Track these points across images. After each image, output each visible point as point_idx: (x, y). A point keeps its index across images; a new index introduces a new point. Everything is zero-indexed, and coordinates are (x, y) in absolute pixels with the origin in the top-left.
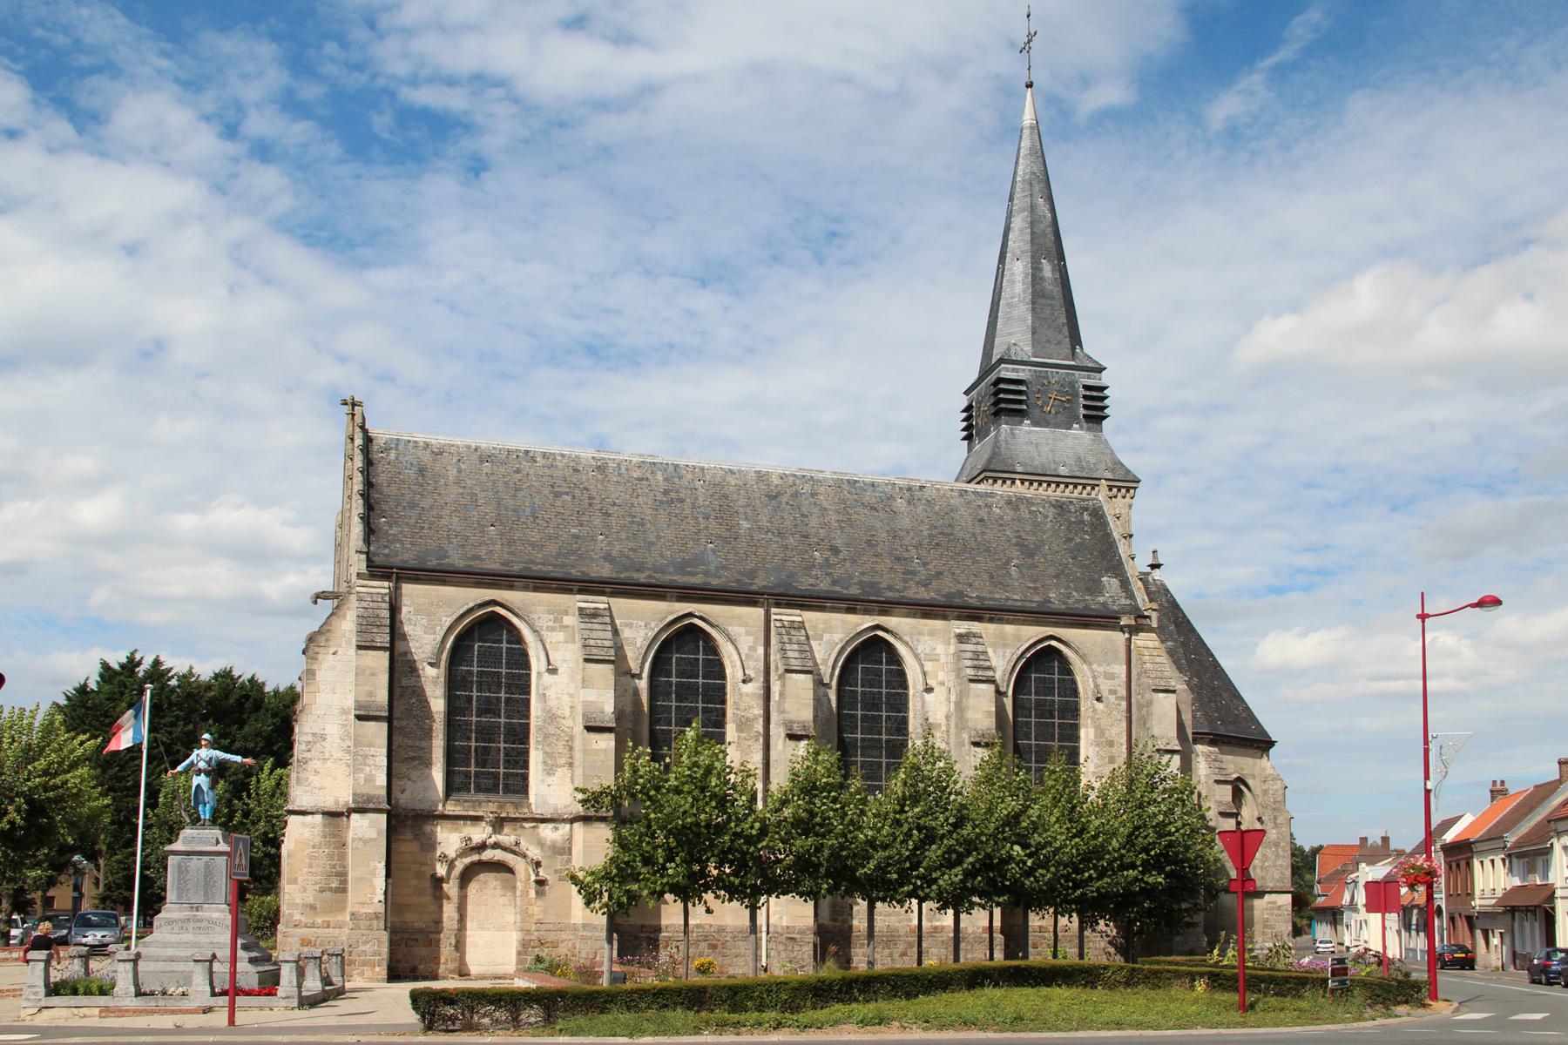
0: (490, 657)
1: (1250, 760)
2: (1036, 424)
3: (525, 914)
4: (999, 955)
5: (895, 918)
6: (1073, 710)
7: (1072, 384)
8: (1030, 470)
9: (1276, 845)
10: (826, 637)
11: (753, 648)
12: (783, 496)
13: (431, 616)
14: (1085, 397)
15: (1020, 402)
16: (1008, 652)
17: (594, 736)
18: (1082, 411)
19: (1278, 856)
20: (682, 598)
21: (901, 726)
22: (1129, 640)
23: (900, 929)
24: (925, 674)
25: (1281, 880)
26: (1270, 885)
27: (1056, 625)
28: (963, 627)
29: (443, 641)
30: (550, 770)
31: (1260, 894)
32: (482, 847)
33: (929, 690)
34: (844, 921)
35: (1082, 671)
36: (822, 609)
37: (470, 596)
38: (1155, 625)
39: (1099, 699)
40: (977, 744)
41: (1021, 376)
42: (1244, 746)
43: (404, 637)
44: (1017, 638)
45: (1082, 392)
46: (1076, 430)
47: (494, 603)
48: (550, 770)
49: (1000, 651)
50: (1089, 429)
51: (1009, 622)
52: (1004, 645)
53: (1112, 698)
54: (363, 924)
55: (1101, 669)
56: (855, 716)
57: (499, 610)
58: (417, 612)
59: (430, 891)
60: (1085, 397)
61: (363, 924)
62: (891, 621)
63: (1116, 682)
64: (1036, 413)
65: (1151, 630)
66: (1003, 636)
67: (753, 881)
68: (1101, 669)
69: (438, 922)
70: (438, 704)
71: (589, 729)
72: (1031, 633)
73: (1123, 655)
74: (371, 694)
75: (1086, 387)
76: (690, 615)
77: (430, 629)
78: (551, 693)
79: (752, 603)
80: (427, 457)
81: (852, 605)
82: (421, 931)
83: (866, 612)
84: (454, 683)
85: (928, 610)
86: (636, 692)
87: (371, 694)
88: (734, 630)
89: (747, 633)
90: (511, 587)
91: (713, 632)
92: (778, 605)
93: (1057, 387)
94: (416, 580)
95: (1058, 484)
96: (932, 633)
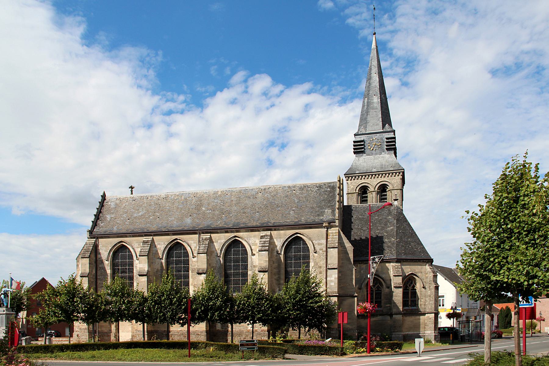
0: (124, 257)
1: (419, 267)
2: (368, 155)
3: (133, 328)
4: (146, 339)
5: (237, 327)
6: (308, 257)
7: (382, 139)
8: (361, 172)
9: (430, 296)
10: (219, 241)
11: (196, 247)
12: (199, 201)
13: (106, 247)
14: (387, 142)
15: (362, 148)
16: (282, 240)
17: (141, 277)
18: (386, 147)
19: (430, 300)
20: (174, 234)
21: (246, 267)
22: (327, 231)
23: (242, 330)
24: (252, 250)
25: (431, 309)
26: (428, 311)
27: (299, 229)
28: (263, 233)
29: (109, 253)
31: (424, 314)
33: (253, 255)
34: (226, 329)
35: (309, 243)
36: (217, 233)
37: (290, 232)
38: (337, 225)
39: (315, 253)
40: (199, 274)
41: (362, 139)
42: (415, 262)
43: (100, 254)
44: (285, 235)
45: (385, 140)
46: (383, 155)
47: (235, 236)
49: (279, 240)
50: (388, 154)
51: (282, 230)
52: (280, 238)
53: (321, 252)
54: (83, 331)
55: (317, 242)
56: (231, 265)
57: (298, 235)
58: (103, 246)
60: (387, 142)
61: (83, 331)
62: (240, 234)
63: (323, 246)
64: (367, 151)
65: (336, 226)
66: (280, 235)
67: (193, 318)
68: (317, 242)
69: (111, 330)
70: (109, 271)
71: (140, 275)
72: (290, 232)
73: (325, 236)
74: (85, 270)
75: (387, 139)
76: (176, 239)
77: (106, 251)
79: (195, 233)
80: (118, 202)
81: (227, 230)
82: (106, 333)
83: (232, 232)
84: (114, 265)
85: (253, 229)
86: (162, 263)
87: (85, 270)
88: (190, 242)
89: (194, 243)
90: (126, 237)
91: (128, 246)
92: (203, 233)
93: (376, 140)
94: (102, 238)
95: (372, 175)
96: (254, 236)
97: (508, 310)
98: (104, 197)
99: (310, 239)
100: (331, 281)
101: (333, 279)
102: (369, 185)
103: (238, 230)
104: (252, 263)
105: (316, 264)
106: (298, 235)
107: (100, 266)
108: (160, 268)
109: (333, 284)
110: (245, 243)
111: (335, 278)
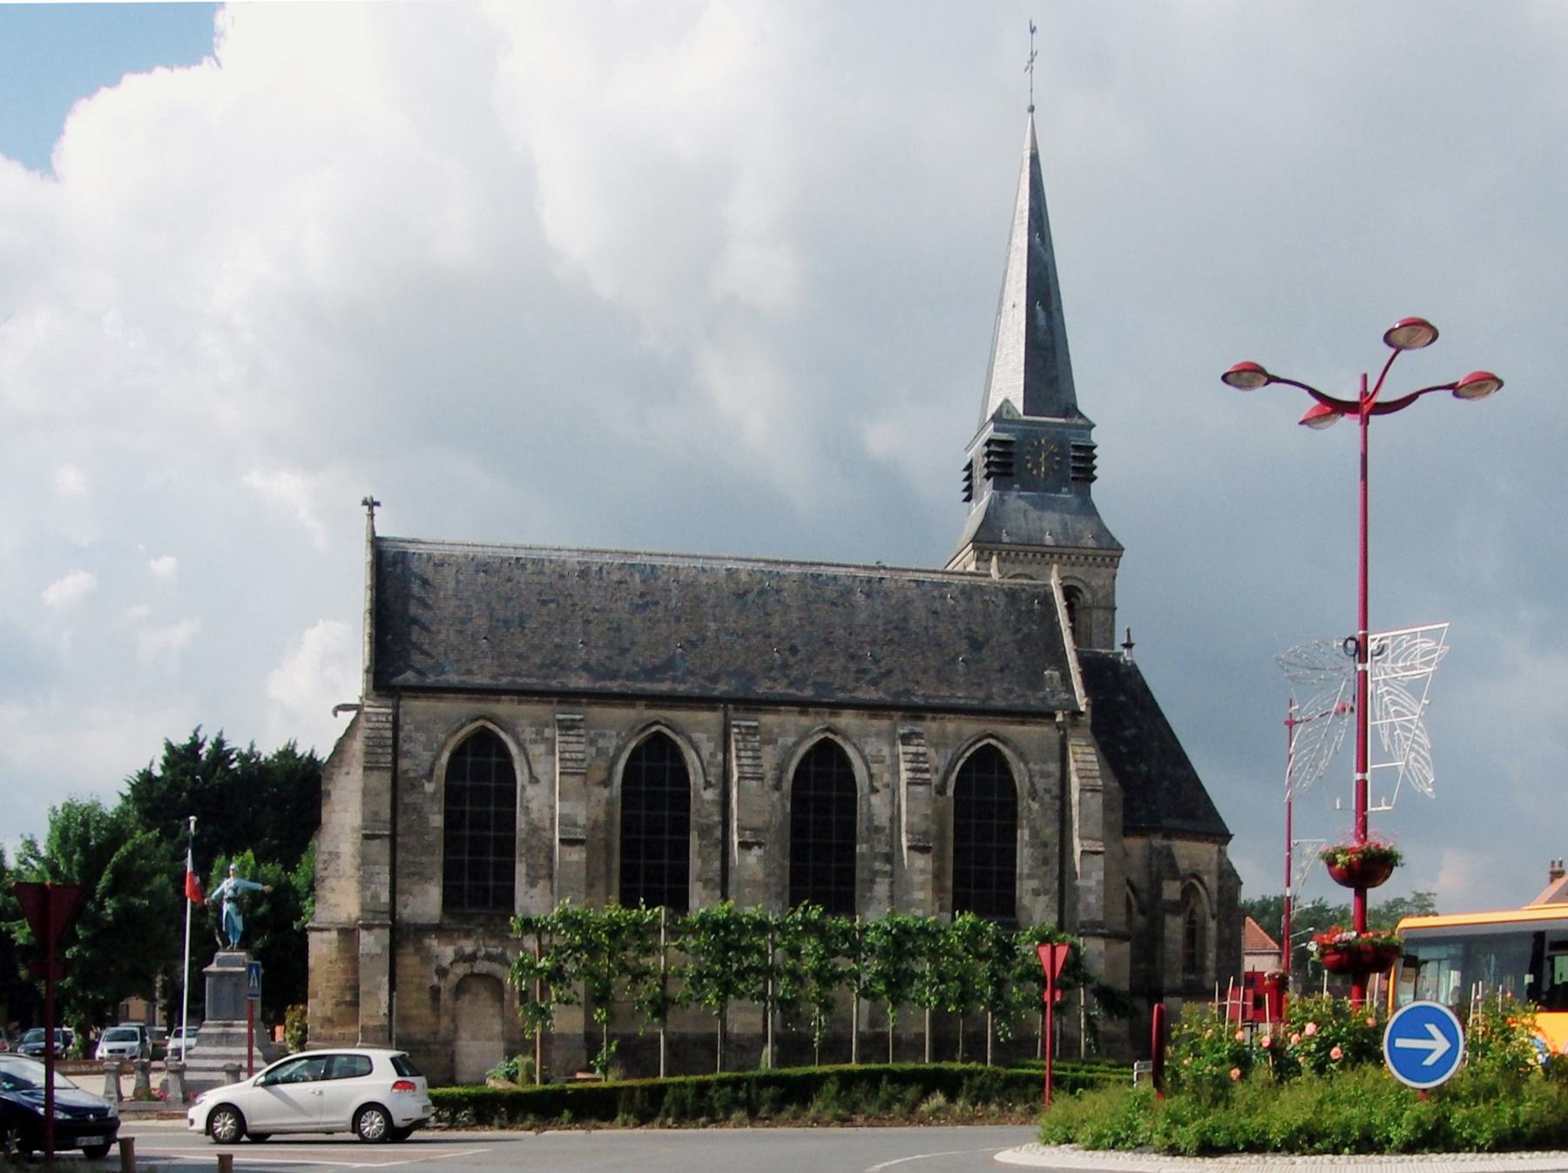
10: (780, 741)
11: (713, 755)
16: (950, 752)
30: (532, 883)
32: (472, 958)
37: (972, 727)
44: (958, 736)
48: (532, 883)
55: (1037, 768)
59: (429, 1003)
73: (1057, 754)
78: (534, 805)
89: (709, 740)
91: (503, 735)
95: (1043, 555)
97: (936, 1057)
98: (1302, 423)
99: (1022, 756)
100: (1089, 890)
101: (1092, 883)
102: (1080, 585)
103: (837, 707)
104: (870, 818)
105: (1035, 833)
106: (993, 742)
107: (407, 799)
108: (602, 818)
109: (1092, 899)
110: (851, 752)
111: (1098, 882)
